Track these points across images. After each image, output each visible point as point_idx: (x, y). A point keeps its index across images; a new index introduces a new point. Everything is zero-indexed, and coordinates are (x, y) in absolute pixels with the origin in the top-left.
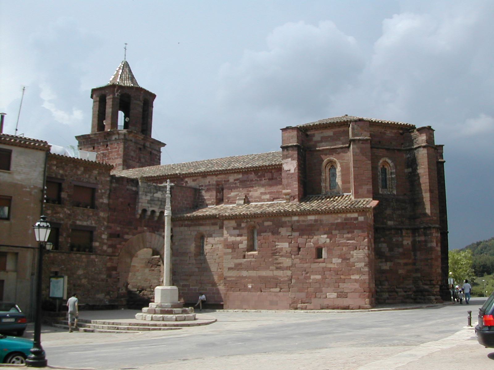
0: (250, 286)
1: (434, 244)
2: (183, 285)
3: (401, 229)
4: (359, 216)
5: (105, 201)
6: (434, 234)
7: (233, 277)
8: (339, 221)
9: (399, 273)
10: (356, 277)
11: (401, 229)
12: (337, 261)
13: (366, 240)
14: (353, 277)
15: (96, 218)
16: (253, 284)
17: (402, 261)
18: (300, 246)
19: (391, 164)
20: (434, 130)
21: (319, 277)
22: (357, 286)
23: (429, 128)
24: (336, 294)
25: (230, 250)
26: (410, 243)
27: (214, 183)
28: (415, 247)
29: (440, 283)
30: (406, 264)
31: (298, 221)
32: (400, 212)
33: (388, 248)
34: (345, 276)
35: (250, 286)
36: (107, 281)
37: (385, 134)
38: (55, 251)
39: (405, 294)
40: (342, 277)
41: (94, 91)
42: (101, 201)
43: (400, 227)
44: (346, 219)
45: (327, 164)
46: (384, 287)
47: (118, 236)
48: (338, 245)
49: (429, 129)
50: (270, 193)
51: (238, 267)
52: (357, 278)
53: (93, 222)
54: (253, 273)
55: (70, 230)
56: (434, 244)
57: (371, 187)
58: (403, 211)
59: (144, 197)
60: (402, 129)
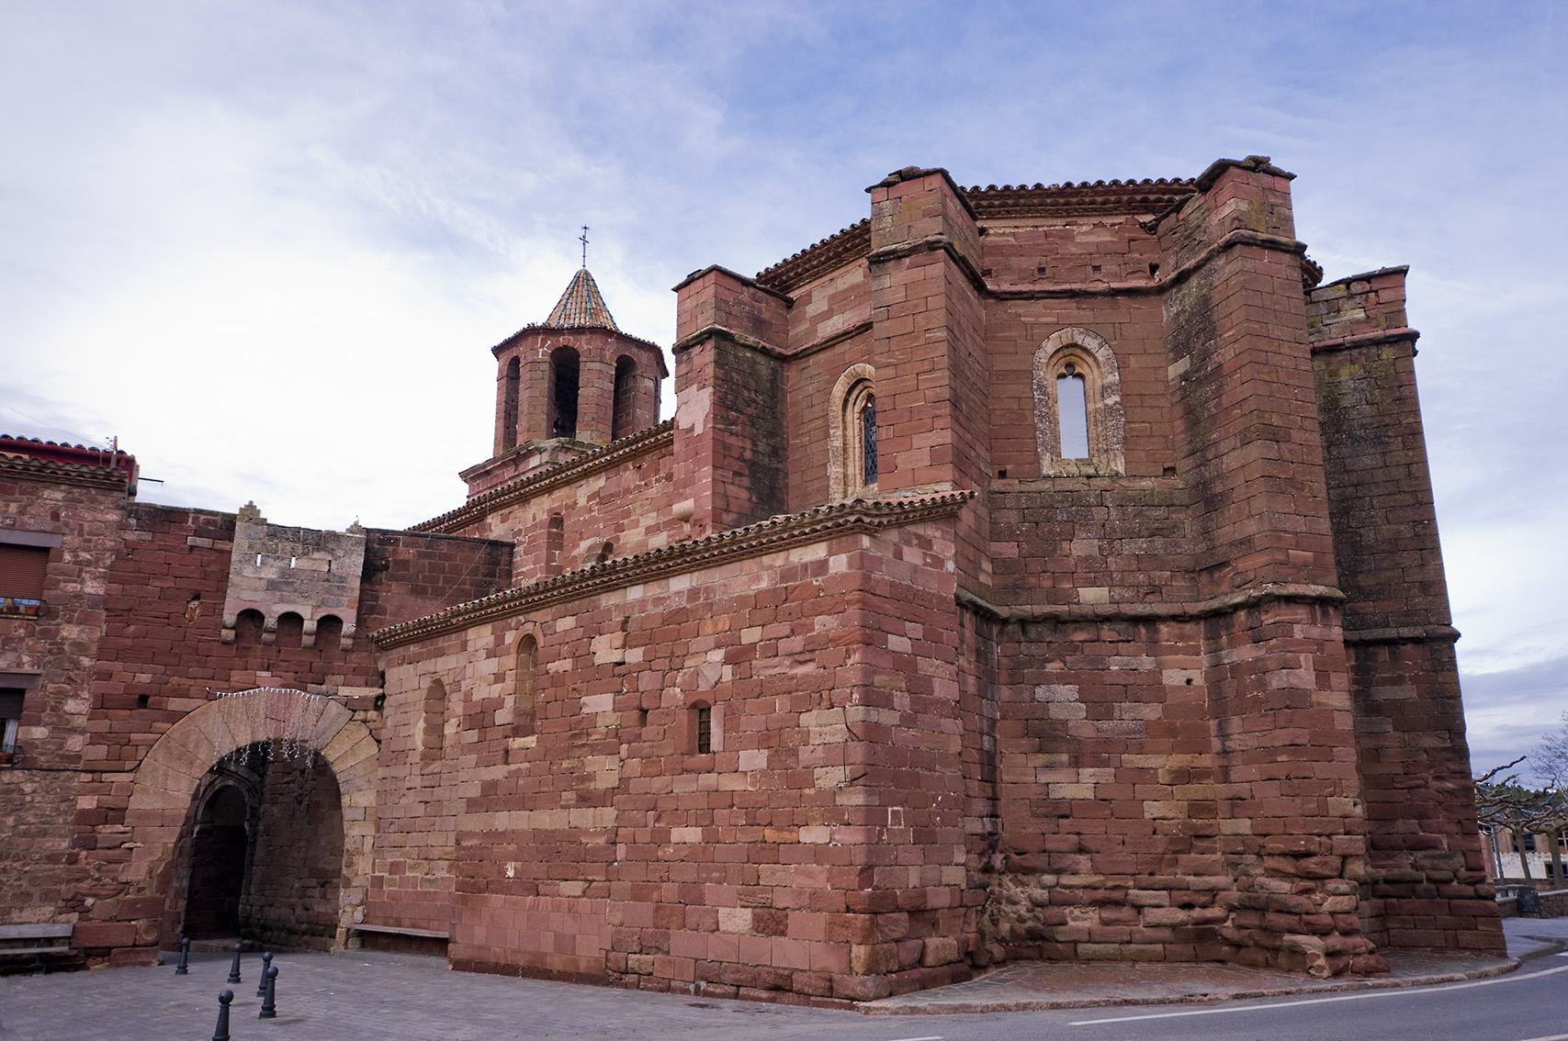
0: (511, 873)
3: (1150, 620)
4: (831, 553)
5: (92, 587)
6: (1297, 628)
12: (755, 759)
13: (856, 657)
15: (43, 645)
17: (1163, 763)
18: (645, 706)
21: (692, 835)
23: (1258, 165)
24: (748, 913)
25: (473, 736)
26: (1199, 680)
27: (545, 516)
28: (1223, 694)
30: (1184, 776)
31: (642, 603)
32: (1143, 543)
34: (780, 829)
36: (73, 860)
37: (1069, 237)
39: (1181, 915)
40: (770, 834)
41: (497, 351)
42: (71, 587)
43: (1140, 609)
44: (788, 573)
47: (143, 701)
48: (758, 690)
49: (1253, 170)
50: (668, 525)
51: (489, 798)
52: (821, 841)
53: (26, 659)
56: (1304, 676)
58: (1159, 542)
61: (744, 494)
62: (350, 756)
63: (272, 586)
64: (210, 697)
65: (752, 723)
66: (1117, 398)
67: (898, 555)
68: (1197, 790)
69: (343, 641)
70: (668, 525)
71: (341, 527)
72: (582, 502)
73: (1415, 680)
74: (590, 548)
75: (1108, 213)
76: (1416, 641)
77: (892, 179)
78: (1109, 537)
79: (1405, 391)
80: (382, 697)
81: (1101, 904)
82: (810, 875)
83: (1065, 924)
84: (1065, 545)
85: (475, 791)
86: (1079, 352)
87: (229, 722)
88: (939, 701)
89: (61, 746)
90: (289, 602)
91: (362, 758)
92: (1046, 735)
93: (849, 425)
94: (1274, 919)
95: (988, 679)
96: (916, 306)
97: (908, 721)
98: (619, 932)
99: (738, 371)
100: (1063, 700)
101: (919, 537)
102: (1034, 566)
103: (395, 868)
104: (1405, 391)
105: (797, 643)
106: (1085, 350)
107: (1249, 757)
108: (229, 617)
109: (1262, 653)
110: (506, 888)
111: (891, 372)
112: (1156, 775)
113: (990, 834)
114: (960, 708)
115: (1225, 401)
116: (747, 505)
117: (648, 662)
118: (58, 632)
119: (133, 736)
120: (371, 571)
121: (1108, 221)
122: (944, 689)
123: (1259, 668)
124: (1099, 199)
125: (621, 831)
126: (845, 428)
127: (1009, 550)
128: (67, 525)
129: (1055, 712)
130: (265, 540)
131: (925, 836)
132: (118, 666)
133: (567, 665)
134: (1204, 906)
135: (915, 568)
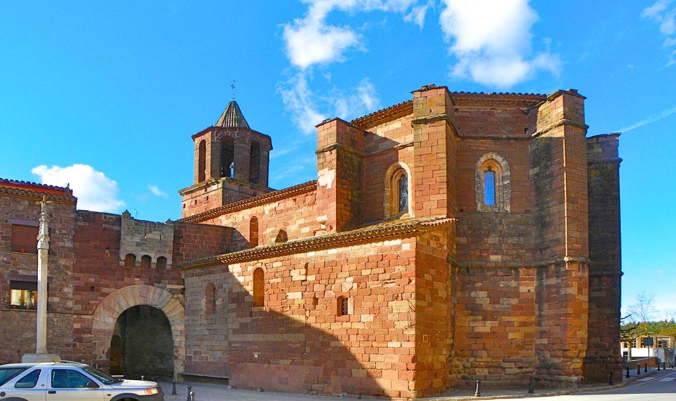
0: (256, 356)
1: (573, 290)
2: (195, 352)
3: (516, 269)
5: (69, 244)
6: (573, 273)
7: (238, 342)
8: (372, 253)
9: (510, 338)
10: (395, 344)
11: (516, 269)
12: (367, 318)
14: (390, 345)
16: (260, 353)
17: (515, 319)
18: (317, 297)
19: (504, 163)
20: (585, 98)
22: (395, 359)
23: (573, 92)
25: (234, 306)
26: (532, 289)
28: (541, 296)
29: (584, 354)
30: (524, 324)
33: (489, 299)
35: (256, 356)
36: (75, 345)
37: (491, 114)
38: (16, 310)
39: (518, 371)
40: (375, 344)
42: (60, 244)
45: (394, 173)
46: (479, 360)
47: (92, 288)
50: (312, 224)
54: (259, 337)
55: (9, 282)
56: (573, 290)
57: (445, 197)
58: (522, 239)
59: (128, 238)
60: (525, 104)
61: (349, 214)
62: (173, 311)
63: (138, 244)
64: (117, 287)
65: (368, 304)
66: (509, 182)
67: (429, 243)
68: (527, 330)
69: (167, 267)
70: (312, 224)
71: (164, 221)
72: (267, 212)
73: (605, 290)
74: (273, 232)
75: (509, 106)
76: (608, 276)
77: (423, 88)
78: (502, 235)
79: (615, 182)
80: (184, 289)
81: (488, 367)
82: (392, 358)
83: (476, 374)
84: (486, 239)
85: (237, 326)
86: (494, 162)
87: (130, 296)
88: (440, 297)
89: (65, 304)
90: (147, 251)
91: (178, 312)
92: (474, 310)
93: (394, 186)
94: (553, 371)
95: (454, 289)
96: (433, 143)
97: (430, 305)
98: (308, 377)
99: (345, 163)
100: (481, 297)
101: (435, 236)
102: (473, 247)
103: (196, 353)
104: (615, 182)
105: (387, 276)
106: (496, 161)
107: (550, 318)
108: (123, 257)
109: (559, 281)
110: (254, 361)
111: (421, 169)
112: (513, 324)
113: (452, 344)
114: (446, 301)
115: (554, 186)
116: (349, 218)
117: (318, 281)
118: (57, 261)
119: (91, 302)
120: (177, 238)
121: (508, 109)
122: (442, 294)
123: (557, 286)
124: (506, 100)
125: (308, 342)
126: (391, 188)
127: (463, 240)
128: (56, 218)
129: (478, 301)
130: (134, 226)
131: (434, 345)
132: (81, 275)
133: (279, 280)
134: (526, 368)
135: (434, 249)
